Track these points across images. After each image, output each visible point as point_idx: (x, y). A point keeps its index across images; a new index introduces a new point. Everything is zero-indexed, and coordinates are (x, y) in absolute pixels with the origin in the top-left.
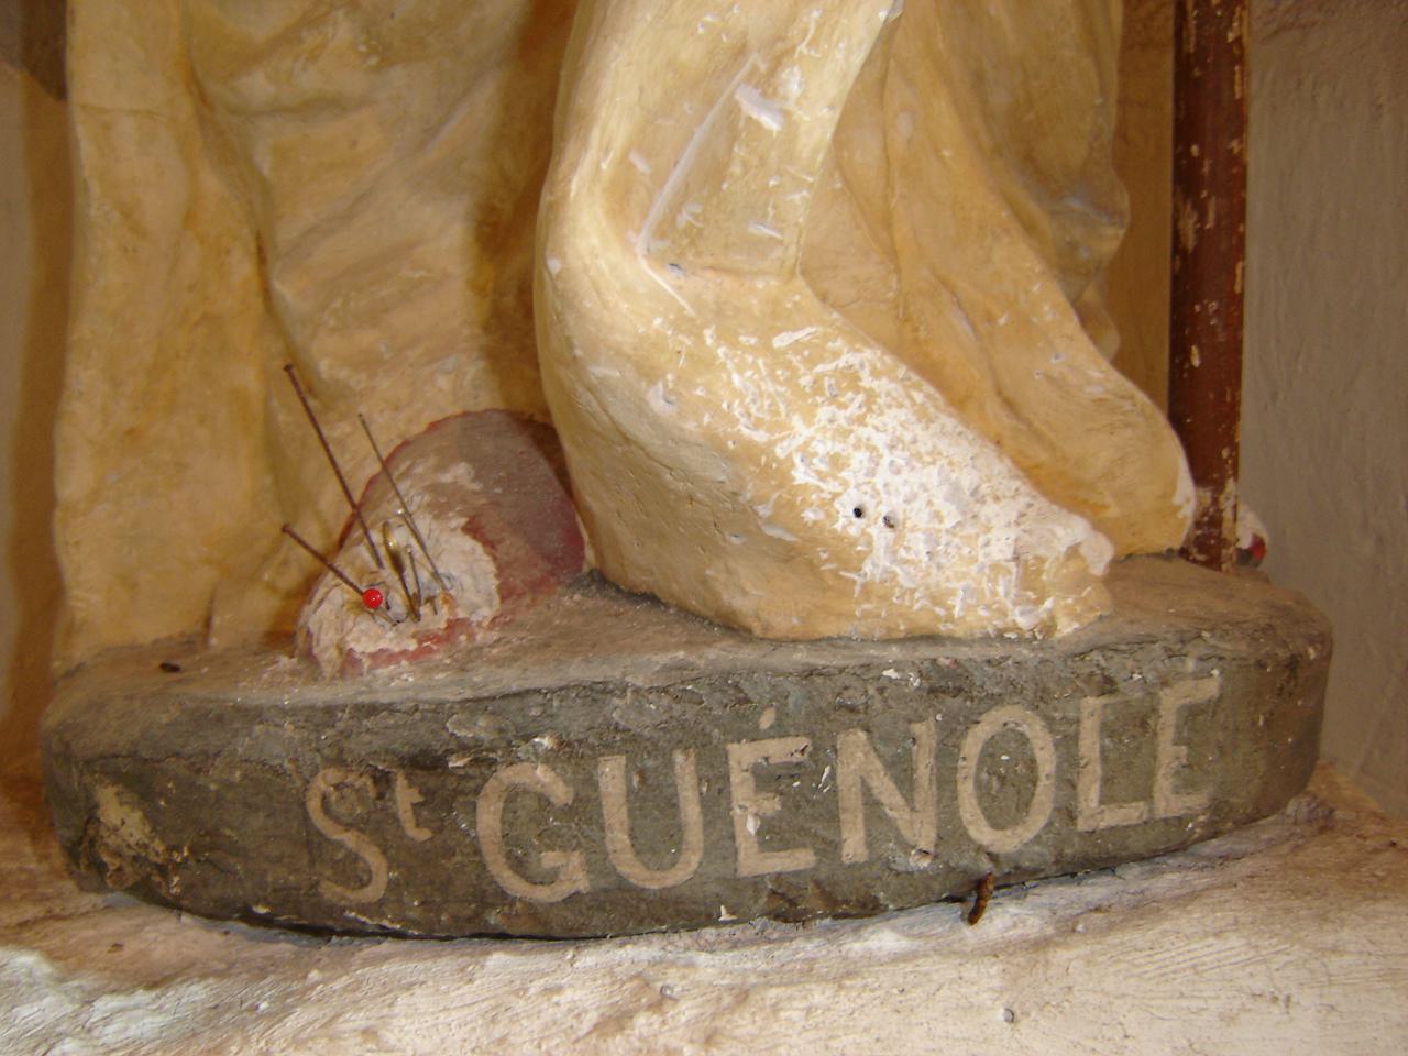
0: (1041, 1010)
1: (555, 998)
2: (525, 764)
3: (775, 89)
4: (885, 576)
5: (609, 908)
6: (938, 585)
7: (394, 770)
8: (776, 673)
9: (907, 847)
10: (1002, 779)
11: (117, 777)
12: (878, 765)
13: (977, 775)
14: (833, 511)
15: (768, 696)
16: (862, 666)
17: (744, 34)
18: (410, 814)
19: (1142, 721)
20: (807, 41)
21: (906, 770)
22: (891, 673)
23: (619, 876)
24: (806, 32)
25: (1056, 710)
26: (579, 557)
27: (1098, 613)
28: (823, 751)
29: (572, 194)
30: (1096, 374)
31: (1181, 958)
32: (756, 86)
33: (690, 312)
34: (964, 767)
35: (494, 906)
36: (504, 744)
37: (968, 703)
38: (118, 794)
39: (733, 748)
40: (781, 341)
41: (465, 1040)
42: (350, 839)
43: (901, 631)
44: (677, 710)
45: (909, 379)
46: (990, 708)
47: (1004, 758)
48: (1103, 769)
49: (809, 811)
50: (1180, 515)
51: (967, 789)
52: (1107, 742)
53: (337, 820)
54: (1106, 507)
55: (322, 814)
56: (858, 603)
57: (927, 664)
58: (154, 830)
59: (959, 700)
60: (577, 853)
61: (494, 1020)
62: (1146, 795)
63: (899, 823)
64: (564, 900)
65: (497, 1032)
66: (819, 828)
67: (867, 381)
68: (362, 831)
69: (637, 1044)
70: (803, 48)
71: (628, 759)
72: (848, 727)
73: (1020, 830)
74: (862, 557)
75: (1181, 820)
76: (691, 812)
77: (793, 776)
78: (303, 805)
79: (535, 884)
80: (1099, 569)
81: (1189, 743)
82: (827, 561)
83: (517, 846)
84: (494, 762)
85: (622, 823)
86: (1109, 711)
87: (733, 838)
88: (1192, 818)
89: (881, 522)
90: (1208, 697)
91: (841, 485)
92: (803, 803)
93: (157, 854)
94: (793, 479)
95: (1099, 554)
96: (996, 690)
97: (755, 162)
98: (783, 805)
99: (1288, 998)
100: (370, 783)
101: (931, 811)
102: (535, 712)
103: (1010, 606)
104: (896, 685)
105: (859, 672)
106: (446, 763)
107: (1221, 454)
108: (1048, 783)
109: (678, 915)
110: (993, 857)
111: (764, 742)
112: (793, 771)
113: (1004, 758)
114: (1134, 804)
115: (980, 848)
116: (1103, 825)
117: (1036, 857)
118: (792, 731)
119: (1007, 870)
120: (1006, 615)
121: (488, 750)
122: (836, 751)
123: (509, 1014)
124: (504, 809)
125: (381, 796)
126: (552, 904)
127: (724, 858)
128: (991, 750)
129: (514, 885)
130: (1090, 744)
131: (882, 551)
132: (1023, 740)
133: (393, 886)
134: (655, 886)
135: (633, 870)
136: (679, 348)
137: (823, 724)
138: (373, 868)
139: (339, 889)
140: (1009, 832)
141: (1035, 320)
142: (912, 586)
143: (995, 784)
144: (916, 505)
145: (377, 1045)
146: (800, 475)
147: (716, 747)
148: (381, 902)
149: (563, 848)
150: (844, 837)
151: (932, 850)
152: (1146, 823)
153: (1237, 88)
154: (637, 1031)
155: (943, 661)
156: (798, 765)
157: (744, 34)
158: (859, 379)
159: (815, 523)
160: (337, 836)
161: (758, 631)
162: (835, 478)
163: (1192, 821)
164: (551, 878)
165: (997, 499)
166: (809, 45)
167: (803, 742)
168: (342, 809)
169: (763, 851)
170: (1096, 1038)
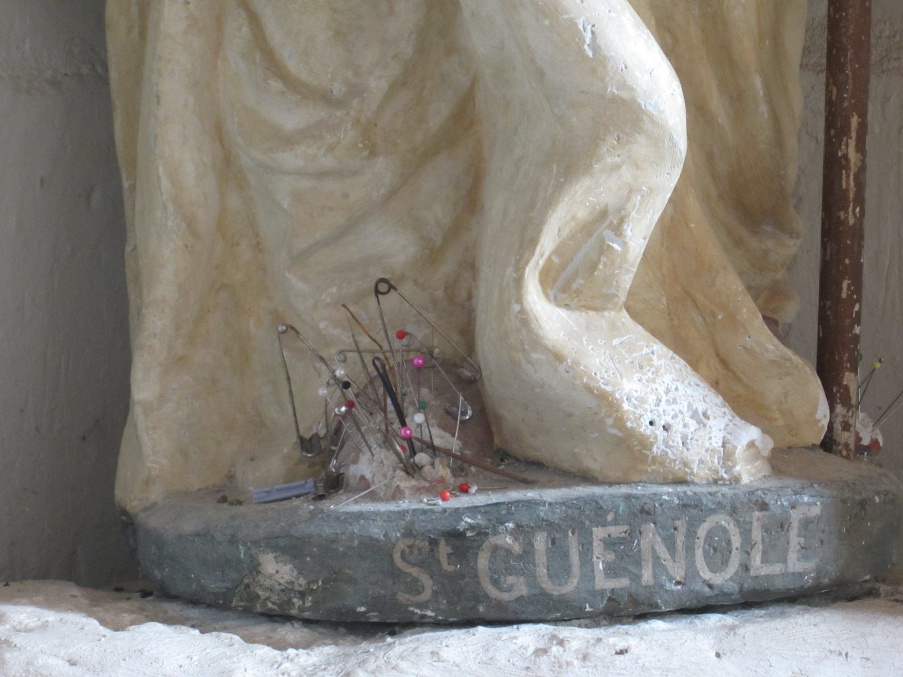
0: (732, 653)
1: (514, 641)
2: (502, 535)
3: (621, 232)
4: (663, 453)
5: (535, 603)
6: (687, 458)
7: (440, 538)
8: (614, 497)
9: (671, 579)
10: (715, 549)
11: (276, 548)
12: (659, 539)
13: (704, 547)
14: (640, 423)
15: (611, 506)
16: (653, 494)
17: (607, 206)
18: (446, 558)
19: (783, 525)
20: (636, 209)
21: (671, 542)
22: (665, 497)
23: (541, 588)
24: (635, 206)
25: (741, 517)
26: (492, 441)
27: (763, 474)
28: (634, 533)
29: (526, 275)
30: (771, 347)
31: (797, 634)
32: (612, 231)
33: (575, 328)
34: (698, 542)
35: (482, 602)
36: (492, 526)
37: (700, 512)
38: (275, 558)
39: (594, 529)
40: (616, 342)
41: (475, 658)
42: (414, 571)
43: (669, 479)
44: (570, 512)
45: (674, 358)
46: (710, 515)
47: (716, 539)
48: (763, 547)
49: (627, 560)
50: (820, 425)
51: (699, 553)
52: (765, 534)
53: (409, 562)
54: (776, 419)
55: (401, 560)
56: (650, 466)
57: (682, 494)
58: (300, 573)
59: (696, 510)
60: (522, 577)
61: (488, 650)
62: (785, 561)
63: (668, 567)
64: (515, 600)
65: (490, 654)
66: (632, 568)
67: (656, 362)
68: (421, 567)
69: (553, 659)
70: (633, 214)
71: (548, 534)
72: (646, 522)
73: (723, 573)
74: (652, 444)
75: (801, 575)
76: (575, 559)
77: (621, 543)
78: (391, 556)
79: (503, 591)
80: (766, 453)
81: (805, 537)
82: (636, 445)
83: (495, 573)
84: (487, 534)
85: (543, 564)
86: (765, 519)
87: (593, 571)
88: (809, 573)
89: (661, 428)
90: (815, 514)
91: (644, 411)
92: (625, 557)
93: (301, 586)
94: (623, 408)
95: (766, 445)
96: (713, 507)
97: (609, 263)
98: (616, 557)
99: (847, 654)
100: (427, 544)
101: (683, 563)
102: (504, 512)
103: (720, 469)
104: (668, 503)
105: (651, 496)
106: (465, 534)
107: (832, 390)
108: (737, 552)
109: (567, 607)
110: (710, 586)
111: (609, 527)
112: (621, 541)
113: (716, 539)
114: (778, 564)
115: (704, 581)
116: (762, 573)
117: (730, 587)
118: (621, 522)
119: (717, 592)
120: (718, 473)
121: (484, 528)
122: (640, 533)
123: (494, 647)
124: (491, 556)
125: (432, 550)
126: (509, 602)
127: (589, 581)
128: (711, 535)
129: (493, 592)
130: (757, 534)
131: (662, 441)
132: (725, 530)
133: (435, 593)
134: (556, 593)
135: (548, 585)
136: (573, 347)
137: (635, 520)
138: (425, 585)
139: (407, 596)
140: (718, 574)
141: (738, 317)
142: (675, 458)
143: (712, 551)
144: (677, 420)
145: (438, 658)
146: (626, 406)
147: (587, 529)
148: (428, 602)
149: (516, 575)
150: (643, 573)
151: (683, 581)
152: (783, 574)
153: (844, 183)
154: (553, 654)
155: (689, 493)
156: (624, 538)
157: (607, 206)
158: (652, 360)
159: (632, 427)
160: (407, 570)
161: (601, 479)
162: (642, 408)
163: (807, 575)
164: (510, 589)
165: (715, 418)
166: (636, 213)
167: (626, 528)
168: (412, 558)
169: (606, 578)
170: (757, 666)
